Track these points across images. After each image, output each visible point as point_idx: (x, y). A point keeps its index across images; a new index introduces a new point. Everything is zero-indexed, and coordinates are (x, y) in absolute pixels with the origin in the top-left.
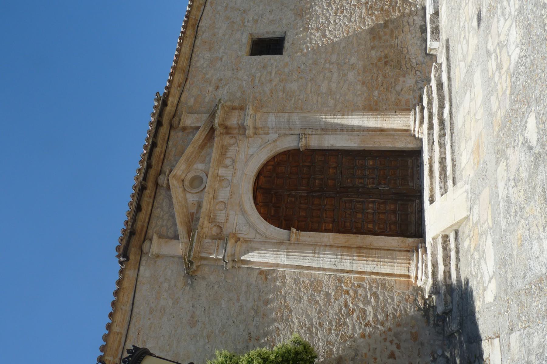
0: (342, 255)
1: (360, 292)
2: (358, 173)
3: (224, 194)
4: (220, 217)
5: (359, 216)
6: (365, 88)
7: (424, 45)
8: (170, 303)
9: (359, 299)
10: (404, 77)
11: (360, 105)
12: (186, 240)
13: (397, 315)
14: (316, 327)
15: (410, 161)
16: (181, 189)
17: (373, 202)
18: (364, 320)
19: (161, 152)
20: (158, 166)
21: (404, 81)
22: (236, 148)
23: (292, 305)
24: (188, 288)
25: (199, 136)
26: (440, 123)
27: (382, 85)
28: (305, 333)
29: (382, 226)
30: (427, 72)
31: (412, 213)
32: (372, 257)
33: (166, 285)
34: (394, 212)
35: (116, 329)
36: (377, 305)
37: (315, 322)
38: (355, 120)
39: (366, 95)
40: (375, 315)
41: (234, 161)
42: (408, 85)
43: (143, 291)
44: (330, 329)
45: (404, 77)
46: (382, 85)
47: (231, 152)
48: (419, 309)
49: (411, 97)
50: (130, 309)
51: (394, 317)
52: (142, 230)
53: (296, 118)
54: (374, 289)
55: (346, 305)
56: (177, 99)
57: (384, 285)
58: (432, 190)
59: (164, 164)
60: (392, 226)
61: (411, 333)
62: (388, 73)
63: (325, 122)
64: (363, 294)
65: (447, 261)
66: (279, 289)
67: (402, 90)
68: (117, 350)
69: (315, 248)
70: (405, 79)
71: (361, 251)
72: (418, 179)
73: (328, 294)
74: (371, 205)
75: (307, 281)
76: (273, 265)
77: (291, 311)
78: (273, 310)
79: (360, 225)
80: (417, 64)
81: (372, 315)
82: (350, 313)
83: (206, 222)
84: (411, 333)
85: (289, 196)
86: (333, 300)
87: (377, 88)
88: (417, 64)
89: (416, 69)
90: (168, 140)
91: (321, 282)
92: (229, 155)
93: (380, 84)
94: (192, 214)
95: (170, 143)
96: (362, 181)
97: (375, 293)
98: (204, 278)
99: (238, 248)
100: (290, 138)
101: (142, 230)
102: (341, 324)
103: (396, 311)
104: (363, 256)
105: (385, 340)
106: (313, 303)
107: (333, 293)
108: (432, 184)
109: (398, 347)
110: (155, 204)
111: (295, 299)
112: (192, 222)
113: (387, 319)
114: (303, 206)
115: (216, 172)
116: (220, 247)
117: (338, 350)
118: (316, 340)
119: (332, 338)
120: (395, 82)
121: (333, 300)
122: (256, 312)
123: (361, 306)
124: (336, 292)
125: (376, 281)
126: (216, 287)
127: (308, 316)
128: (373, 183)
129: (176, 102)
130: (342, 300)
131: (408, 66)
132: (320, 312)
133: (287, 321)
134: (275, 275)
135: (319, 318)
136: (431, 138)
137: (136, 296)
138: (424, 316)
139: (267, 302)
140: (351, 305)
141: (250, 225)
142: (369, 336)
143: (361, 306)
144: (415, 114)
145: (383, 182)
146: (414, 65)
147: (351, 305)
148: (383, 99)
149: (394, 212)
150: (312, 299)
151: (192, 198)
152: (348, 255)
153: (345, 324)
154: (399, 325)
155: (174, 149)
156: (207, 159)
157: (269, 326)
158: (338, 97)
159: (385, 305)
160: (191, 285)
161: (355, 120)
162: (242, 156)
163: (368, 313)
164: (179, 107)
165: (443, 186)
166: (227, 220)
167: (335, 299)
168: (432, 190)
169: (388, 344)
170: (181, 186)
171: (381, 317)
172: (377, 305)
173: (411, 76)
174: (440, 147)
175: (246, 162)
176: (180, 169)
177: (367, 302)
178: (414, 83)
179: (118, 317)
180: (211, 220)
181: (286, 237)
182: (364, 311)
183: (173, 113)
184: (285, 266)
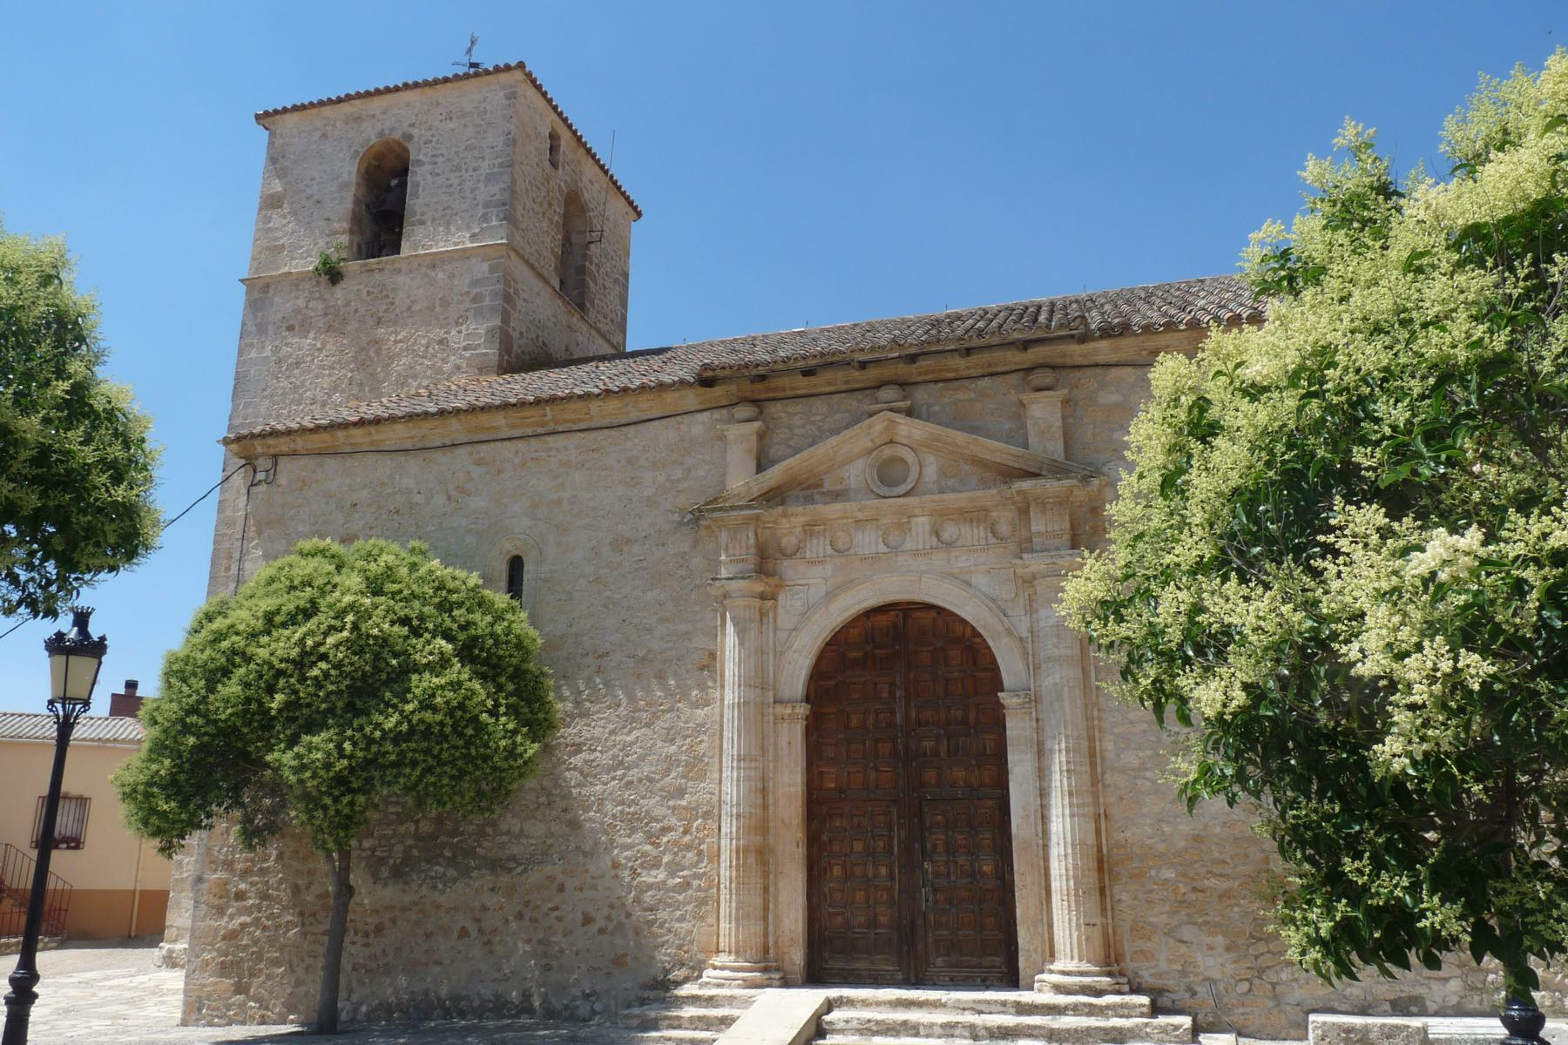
0: (738, 815)
1: (689, 855)
2: (960, 838)
3: (868, 542)
4: (818, 547)
5: (858, 846)
6: (1182, 844)
7: (1344, 1007)
8: (649, 492)
9: (676, 854)
10: (1228, 949)
11: (1128, 834)
12: (756, 492)
13: (654, 929)
14: (625, 775)
15: (998, 960)
16: (869, 444)
17: (891, 875)
18: (642, 866)
19: (956, 370)
20: (920, 374)
21: (1211, 948)
22: (983, 542)
23: (660, 725)
24: (677, 517)
25: (998, 451)
26: (1006, 1028)
27: (1194, 889)
28: (614, 757)
29: (838, 896)
30: (1247, 1010)
31: (873, 963)
32: (738, 877)
33: (679, 473)
34: (873, 923)
35: (594, 407)
36: (668, 890)
37: (633, 774)
38: (1060, 824)
39: (1161, 847)
40: (650, 886)
41: (949, 545)
42: (1199, 958)
43: (664, 433)
44: (622, 803)
45: (1228, 949)
46: (1194, 889)
47: (973, 534)
48: (667, 972)
49: (1164, 966)
50: (634, 419)
51: (651, 923)
52: (774, 390)
53: (1057, 676)
54: (696, 883)
55: (665, 830)
56: (1113, 358)
57: (703, 902)
58: (865, 1003)
59: (931, 385)
60: (840, 919)
61: (625, 955)
62: (1238, 905)
63: (1052, 751)
64: (686, 862)
65: (700, 1025)
66: (685, 696)
67: (1181, 941)
68: (566, 421)
69: (758, 756)
70: (1220, 949)
71: (759, 855)
72: (952, 979)
73: (681, 792)
74: (883, 871)
75: (703, 748)
76: (722, 675)
77: (648, 725)
78: (649, 691)
79: (836, 848)
80: (1274, 985)
81: (650, 880)
82: (652, 838)
83: (802, 519)
84: (625, 955)
85: (893, 684)
86: (671, 803)
87: (1184, 875)
88: (1274, 985)
89: (1256, 981)
90: (992, 375)
91: (702, 777)
92: (966, 530)
93: (1198, 885)
94: (819, 485)
95: (986, 382)
96: (940, 849)
97: (689, 884)
98: (695, 544)
99: (741, 602)
100: (1020, 666)
101: (774, 390)
102: (633, 822)
103: (661, 926)
104: (738, 859)
105: (611, 906)
106: (665, 765)
107: (684, 803)
108: (879, 1004)
109: (602, 931)
110: (837, 397)
111: (669, 729)
112: (806, 488)
113: (646, 910)
114: (871, 720)
115: (918, 511)
116: (739, 567)
117: (591, 820)
118: (605, 778)
119: (609, 807)
120: (1207, 923)
121: (671, 803)
122: (643, 659)
123: (665, 860)
124: (685, 808)
125: (710, 887)
126: (682, 572)
127: (642, 758)
128: (936, 875)
129: (1101, 359)
130: (674, 821)
131: (1266, 960)
132: (651, 780)
133: (631, 721)
134: (710, 684)
135: (640, 780)
136: (993, 1008)
137: (656, 423)
138: (655, 979)
139: (661, 676)
140: (665, 839)
141: (808, 611)
142: (617, 876)
143: (665, 860)
144: (1082, 974)
145: (941, 897)
146: (1271, 976)
147: (665, 839)
148: (1151, 891)
149: (873, 923)
150: (671, 761)
151: (856, 473)
152: (738, 828)
153: (633, 830)
154: (637, 932)
155: (972, 395)
156: (951, 482)
157: (621, 687)
158: (1149, 774)
159: (669, 905)
160: (681, 524)
161: (1060, 824)
162: (963, 562)
163: (654, 872)
164: (1090, 372)
165: (850, 1026)
166: (812, 563)
167: (674, 808)
168: (865, 1003)
169: (606, 911)
170: (879, 442)
171: (648, 897)
172: (668, 890)
173: (1230, 967)
174: (944, 1026)
175: (950, 575)
176: (909, 429)
177: (673, 869)
178: (1208, 974)
179: (613, 404)
180: (810, 529)
181: (786, 693)
182: (656, 864)
183: (1069, 361)
184: (722, 700)
